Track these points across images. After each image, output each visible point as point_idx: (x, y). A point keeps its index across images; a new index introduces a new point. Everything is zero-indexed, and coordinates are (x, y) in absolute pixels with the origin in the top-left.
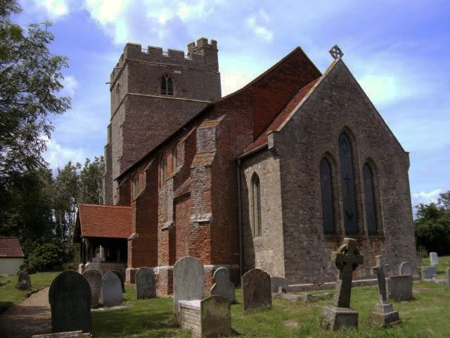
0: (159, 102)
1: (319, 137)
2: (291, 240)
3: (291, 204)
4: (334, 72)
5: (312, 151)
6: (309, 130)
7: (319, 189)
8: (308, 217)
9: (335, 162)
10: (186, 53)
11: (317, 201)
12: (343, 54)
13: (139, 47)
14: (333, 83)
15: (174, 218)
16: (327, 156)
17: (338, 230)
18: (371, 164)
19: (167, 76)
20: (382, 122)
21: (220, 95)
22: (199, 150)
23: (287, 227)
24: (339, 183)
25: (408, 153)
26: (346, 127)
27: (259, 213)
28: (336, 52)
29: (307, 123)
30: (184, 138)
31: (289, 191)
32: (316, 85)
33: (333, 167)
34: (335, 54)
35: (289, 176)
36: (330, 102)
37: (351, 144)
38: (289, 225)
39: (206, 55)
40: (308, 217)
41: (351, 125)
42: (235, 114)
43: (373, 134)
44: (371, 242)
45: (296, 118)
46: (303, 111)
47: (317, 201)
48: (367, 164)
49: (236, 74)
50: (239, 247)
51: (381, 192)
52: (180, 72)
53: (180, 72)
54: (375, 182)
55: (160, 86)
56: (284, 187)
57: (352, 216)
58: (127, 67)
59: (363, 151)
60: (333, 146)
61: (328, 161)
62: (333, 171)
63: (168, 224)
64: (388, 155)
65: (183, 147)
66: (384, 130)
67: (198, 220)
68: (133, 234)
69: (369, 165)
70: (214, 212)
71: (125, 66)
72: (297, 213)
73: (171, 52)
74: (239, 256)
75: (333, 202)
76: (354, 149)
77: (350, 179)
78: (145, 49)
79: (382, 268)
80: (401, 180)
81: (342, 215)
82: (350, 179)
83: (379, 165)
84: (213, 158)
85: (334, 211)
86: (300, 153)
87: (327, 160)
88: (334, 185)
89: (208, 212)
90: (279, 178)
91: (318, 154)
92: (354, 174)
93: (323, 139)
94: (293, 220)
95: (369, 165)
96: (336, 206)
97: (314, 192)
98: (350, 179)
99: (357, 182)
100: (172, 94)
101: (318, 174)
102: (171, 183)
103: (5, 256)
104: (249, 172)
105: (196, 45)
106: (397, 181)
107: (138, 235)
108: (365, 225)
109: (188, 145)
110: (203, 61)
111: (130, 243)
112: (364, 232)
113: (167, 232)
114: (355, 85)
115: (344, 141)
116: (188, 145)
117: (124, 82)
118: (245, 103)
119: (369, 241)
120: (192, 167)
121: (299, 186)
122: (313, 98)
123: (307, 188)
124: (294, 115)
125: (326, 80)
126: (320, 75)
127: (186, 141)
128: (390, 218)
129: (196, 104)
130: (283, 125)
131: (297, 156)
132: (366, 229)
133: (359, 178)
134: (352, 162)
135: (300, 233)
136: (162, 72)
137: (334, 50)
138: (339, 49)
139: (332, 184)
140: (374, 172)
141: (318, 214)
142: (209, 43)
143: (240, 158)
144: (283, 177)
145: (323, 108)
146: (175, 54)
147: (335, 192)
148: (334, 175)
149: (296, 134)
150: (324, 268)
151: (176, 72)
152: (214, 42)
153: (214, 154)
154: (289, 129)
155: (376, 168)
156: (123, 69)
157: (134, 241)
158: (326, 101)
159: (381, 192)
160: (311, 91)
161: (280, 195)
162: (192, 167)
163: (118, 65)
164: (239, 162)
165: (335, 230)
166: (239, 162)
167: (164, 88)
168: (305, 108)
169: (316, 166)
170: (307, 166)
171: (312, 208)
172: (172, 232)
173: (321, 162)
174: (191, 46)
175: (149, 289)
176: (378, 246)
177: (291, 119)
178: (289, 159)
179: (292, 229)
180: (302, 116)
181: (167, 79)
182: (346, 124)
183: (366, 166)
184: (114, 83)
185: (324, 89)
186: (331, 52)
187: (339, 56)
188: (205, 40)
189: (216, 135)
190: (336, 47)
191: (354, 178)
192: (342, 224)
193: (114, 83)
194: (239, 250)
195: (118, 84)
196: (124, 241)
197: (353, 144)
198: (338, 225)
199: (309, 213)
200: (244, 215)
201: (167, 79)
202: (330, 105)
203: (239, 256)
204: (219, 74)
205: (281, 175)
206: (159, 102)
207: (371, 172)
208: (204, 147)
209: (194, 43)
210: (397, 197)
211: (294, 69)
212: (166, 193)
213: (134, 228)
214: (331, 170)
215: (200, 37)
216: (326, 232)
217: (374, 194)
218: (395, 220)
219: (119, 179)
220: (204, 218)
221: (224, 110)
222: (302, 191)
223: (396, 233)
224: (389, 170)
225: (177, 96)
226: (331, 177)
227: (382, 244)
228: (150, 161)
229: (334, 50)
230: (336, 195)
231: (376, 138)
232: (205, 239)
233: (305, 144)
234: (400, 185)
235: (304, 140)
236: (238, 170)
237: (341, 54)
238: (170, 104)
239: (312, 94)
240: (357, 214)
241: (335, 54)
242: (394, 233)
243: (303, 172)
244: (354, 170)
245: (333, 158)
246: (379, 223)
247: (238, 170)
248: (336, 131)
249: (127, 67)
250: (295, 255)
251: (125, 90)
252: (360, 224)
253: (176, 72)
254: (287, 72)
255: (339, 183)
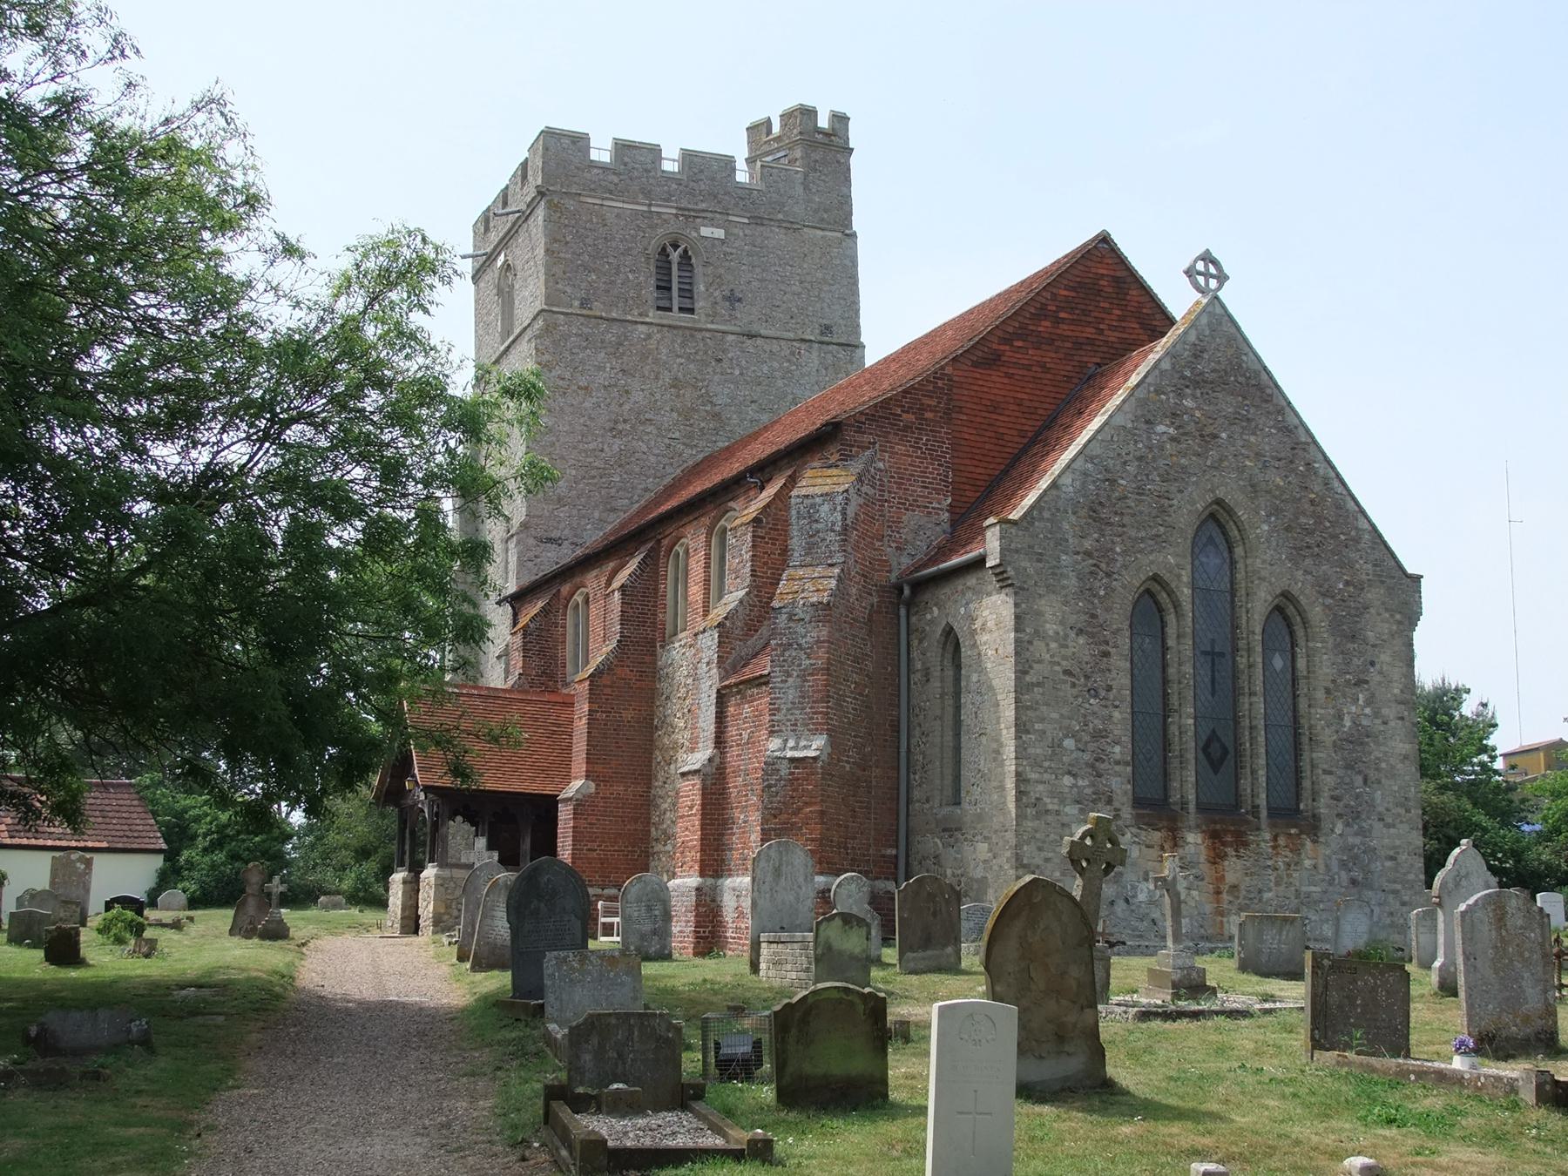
0: (649, 336)
1: (1133, 533)
2: (1037, 816)
3: (1042, 720)
4: (1192, 338)
5: (1108, 575)
6: (1104, 513)
7: (1122, 681)
8: (1087, 757)
9: (1177, 606)
10: (741, 164)
11: (1116, 714)
12: (1226, 278)
13: (579, 141)
14: (1188, 373)
15: (720, 741)
16: (1156, 588)
17: (1175, 797)
18: (1291, 610)
19: (675, 246)
20: (1336, 484)
21: (854, 346)
22: (796, 557)
23: (1027, 781)
24: (1184, 663)
25: (1417, 579)
26: (1219, 502)
27: (957, 735)
28: (1207, 275)
29: (1098, 501)
30: (754, 508)
31: (1038, 684)
32: (1152, 358)
33: (1171, 618)
34: (1201, 279)
35: (1039, 644)
36: (1171, 430)
37: (1231, 550)
38: (1034, 776)
39: (812, 167)
40: (1087, 757)
41: (1233, 494)
42: (899, 448)
43: (1303, 520)
44: (1275, 838)
45: (1067, 480)
46: (1091, 459)
47: (1116, 714)
48: (1279, 609)
49: (915, 285)
50: (897, 831)
51: (1320, 695)
52: (720, 233)
53: (720, 233)
54: (1301, 663)
55: (652, 281)
56: (1026, 673)
57: (1220, 753)
58: (540, 213)
59: (1267, 570)
60: (1173, 562)
61: (1156, 602)
62: (1171, 631)
63: (698, 758)
64: (1347, 583)
65: (749, 537)
66: (1339, 506)
67: (789, 754)
68: (577, 784)
69: (1284, 612)
70: (832, 734)
71: (532, 206)
72: (1056, 746)
73: (689, 157)
74: (896, 857)
75: (1165, 717)
76: (1240, 566)
77: (1219, 660)
78: (601, 153)
79: (1174, 878)
80: (1385, 657)
81: (1191, 756)
82: (1219, 660)
83: (1316, 613)
84: (833, 583)
85: (1166, 745)
86: (1074, 581)
87: (1152, 603)
88: (1172, 671)
89: (814, 732)
90: (1011, 648)
91: (1129, 582)
92: (1235, 639)
93: (1142, 540)
94: (1046, 764)
95: (1284, 612)
96: (1174, 729)
97: (1109, 688)
98: (1222, 655)
99: (1242, 661)
100: (691, 311)
101: (1124, 641)
102: (710, 642)
103: (105, 845)
104: (935, 615)
105: (776, 129)
106: (1372, 664)
107: (593, 785)
108: (1257, 785)
109: (761, 532)
110: (800, 190)
111: (565, 814)
112: (1256, 807)
113: (697, 781)
114: (1257, 373)
115: (1211, 540)
116: (761, 532)
117: (531, 250)
118: (929, 415)
119: (1267, 836)
120: (776, 604)
121: (1067, 672)
122: (1119, 420)
123: (1087, 677)
124: (1063, 472)
125: (1166, 365)
126: (1170, 321)
127: (756, 521)
128: (1340, 772)
129: (775, 347)
130: (1030, 499)
131: (1063, 587)
132: (1262, 800)
133: (1249, 650)
134: (1233, 602)
135: (1062, 802)
136: (660, 231)
137: (1200, 266)
138: (1215, 262)
139: (1164, 667)
140: (1300, 633)
141: (1117, 749)
142: (823, 122)
143: (908, 583)
144: (1020, 648)
145: (1150, 448)
146: (704, 170)
147: (1173, 689)
148: (1171, 642)
149: (1066, 526)
150: (1127, 901)
151: (705, 231)
152: (840, 120)
153: (837, 571)
154: (1046, 515)
155: (1305, 623)
156: (525, 216)
157: (581, 806)
158: (1160, 428)
159: (1320, 695)
160: (1117, 400)
161: (1012, 695)
162: (776, 604)
163: (504, 197)
164: (907, 591)
165: (1166, 796)
166: (907, 591)
167: (664, 287)
168: (1096, 449)
169: (1118, 617)
170: (1093, 616)
171: (1098, 735)
172: (715, 784)
173: (1136, 604)
174: (757, 131)
175: (654, 932)
176: (1297, 851)
177: (1054, 485)
178: (1041, 596)
179: (1040, 787)
180: (1085, 474)
181: (675, 256)
182: (1220, 493)
183: (1278, 618)
184: (490, 258)
185: (1158, 392)
186: (1190, 273)
187: (1213, 283)
188: (808, 113)
189: (844, 514)
190: (1207, 258)
191: (1235, 650)
192: (1186, 784)
193: (490, 258)
194: (897, 841)
195: (507, 267)
196: (546, 806)
197: (1239, 551)
198: (1176, 784)
199: (1092, 746)
200: (913, 741)
201: (675, 256)
202: (1173, 439)
203: (896, 857)
204: (854, 235)
205: (1016, 641)
206: (649, 336)
207: (1292, 634)
208: (810, 548)
209: (768, 122)
210: (1367, 711)
211: (1088, 307)
212: (692, 663)
213: (579, 764)
214: (1163, 624)
215: (791, 103)
216: (1138, 802)
217: (1295, 697)
218: (1359, 780)
219: (517, 600)
220: (805, 747)
221: (867, 438)
222: (1074, 685)
223: (1357, 816)
224: (1348, 634)
225: (713, 316)
226: (1165, 649)
227: (1308, 843)
228: (632, 555)
229: (1200, 266)
230: (1174, 700)
231: (1310, 533)
232: (806, 804)
233: (1088, 554)
234: (1380, 673)
235: (1088, 544)
236: (903, 612)
237: (1222, 278)
238: (683, 345)
239: (1119, 408)
240: (1238, 754)
241: (1201, 279)
242: (1352, 816)
243: (1080, 632)
244: (1235, 627)
245: (1170, 593)
246: (1307, 784)
247: (903, 612)
248: (1188, 507)
249: (540, 213)
250: (1047, 860)
251: (530, 297)
252: (1246, 783)
253: (705, 231)
254: (1062, 315)
255: (1184, 663)
